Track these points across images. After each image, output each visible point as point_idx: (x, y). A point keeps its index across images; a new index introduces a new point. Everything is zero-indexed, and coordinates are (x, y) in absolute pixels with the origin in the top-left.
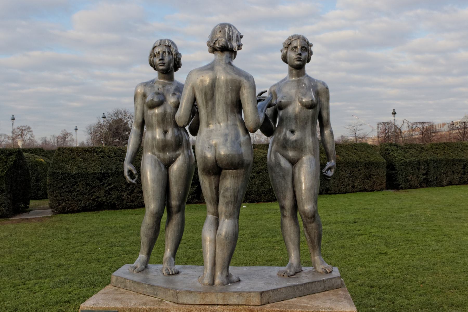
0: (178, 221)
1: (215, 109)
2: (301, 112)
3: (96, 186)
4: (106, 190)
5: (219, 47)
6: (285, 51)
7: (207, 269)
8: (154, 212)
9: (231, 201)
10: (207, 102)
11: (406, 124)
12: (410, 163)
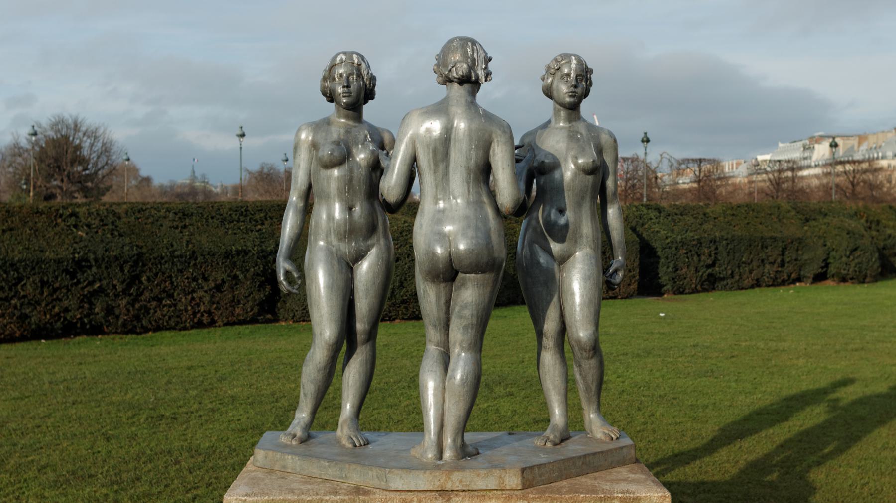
3: (63, 288)
4: (83, 295)
6: (549, 80)
7: (430, 434)
10: (436, 165)
12: (683, 243)
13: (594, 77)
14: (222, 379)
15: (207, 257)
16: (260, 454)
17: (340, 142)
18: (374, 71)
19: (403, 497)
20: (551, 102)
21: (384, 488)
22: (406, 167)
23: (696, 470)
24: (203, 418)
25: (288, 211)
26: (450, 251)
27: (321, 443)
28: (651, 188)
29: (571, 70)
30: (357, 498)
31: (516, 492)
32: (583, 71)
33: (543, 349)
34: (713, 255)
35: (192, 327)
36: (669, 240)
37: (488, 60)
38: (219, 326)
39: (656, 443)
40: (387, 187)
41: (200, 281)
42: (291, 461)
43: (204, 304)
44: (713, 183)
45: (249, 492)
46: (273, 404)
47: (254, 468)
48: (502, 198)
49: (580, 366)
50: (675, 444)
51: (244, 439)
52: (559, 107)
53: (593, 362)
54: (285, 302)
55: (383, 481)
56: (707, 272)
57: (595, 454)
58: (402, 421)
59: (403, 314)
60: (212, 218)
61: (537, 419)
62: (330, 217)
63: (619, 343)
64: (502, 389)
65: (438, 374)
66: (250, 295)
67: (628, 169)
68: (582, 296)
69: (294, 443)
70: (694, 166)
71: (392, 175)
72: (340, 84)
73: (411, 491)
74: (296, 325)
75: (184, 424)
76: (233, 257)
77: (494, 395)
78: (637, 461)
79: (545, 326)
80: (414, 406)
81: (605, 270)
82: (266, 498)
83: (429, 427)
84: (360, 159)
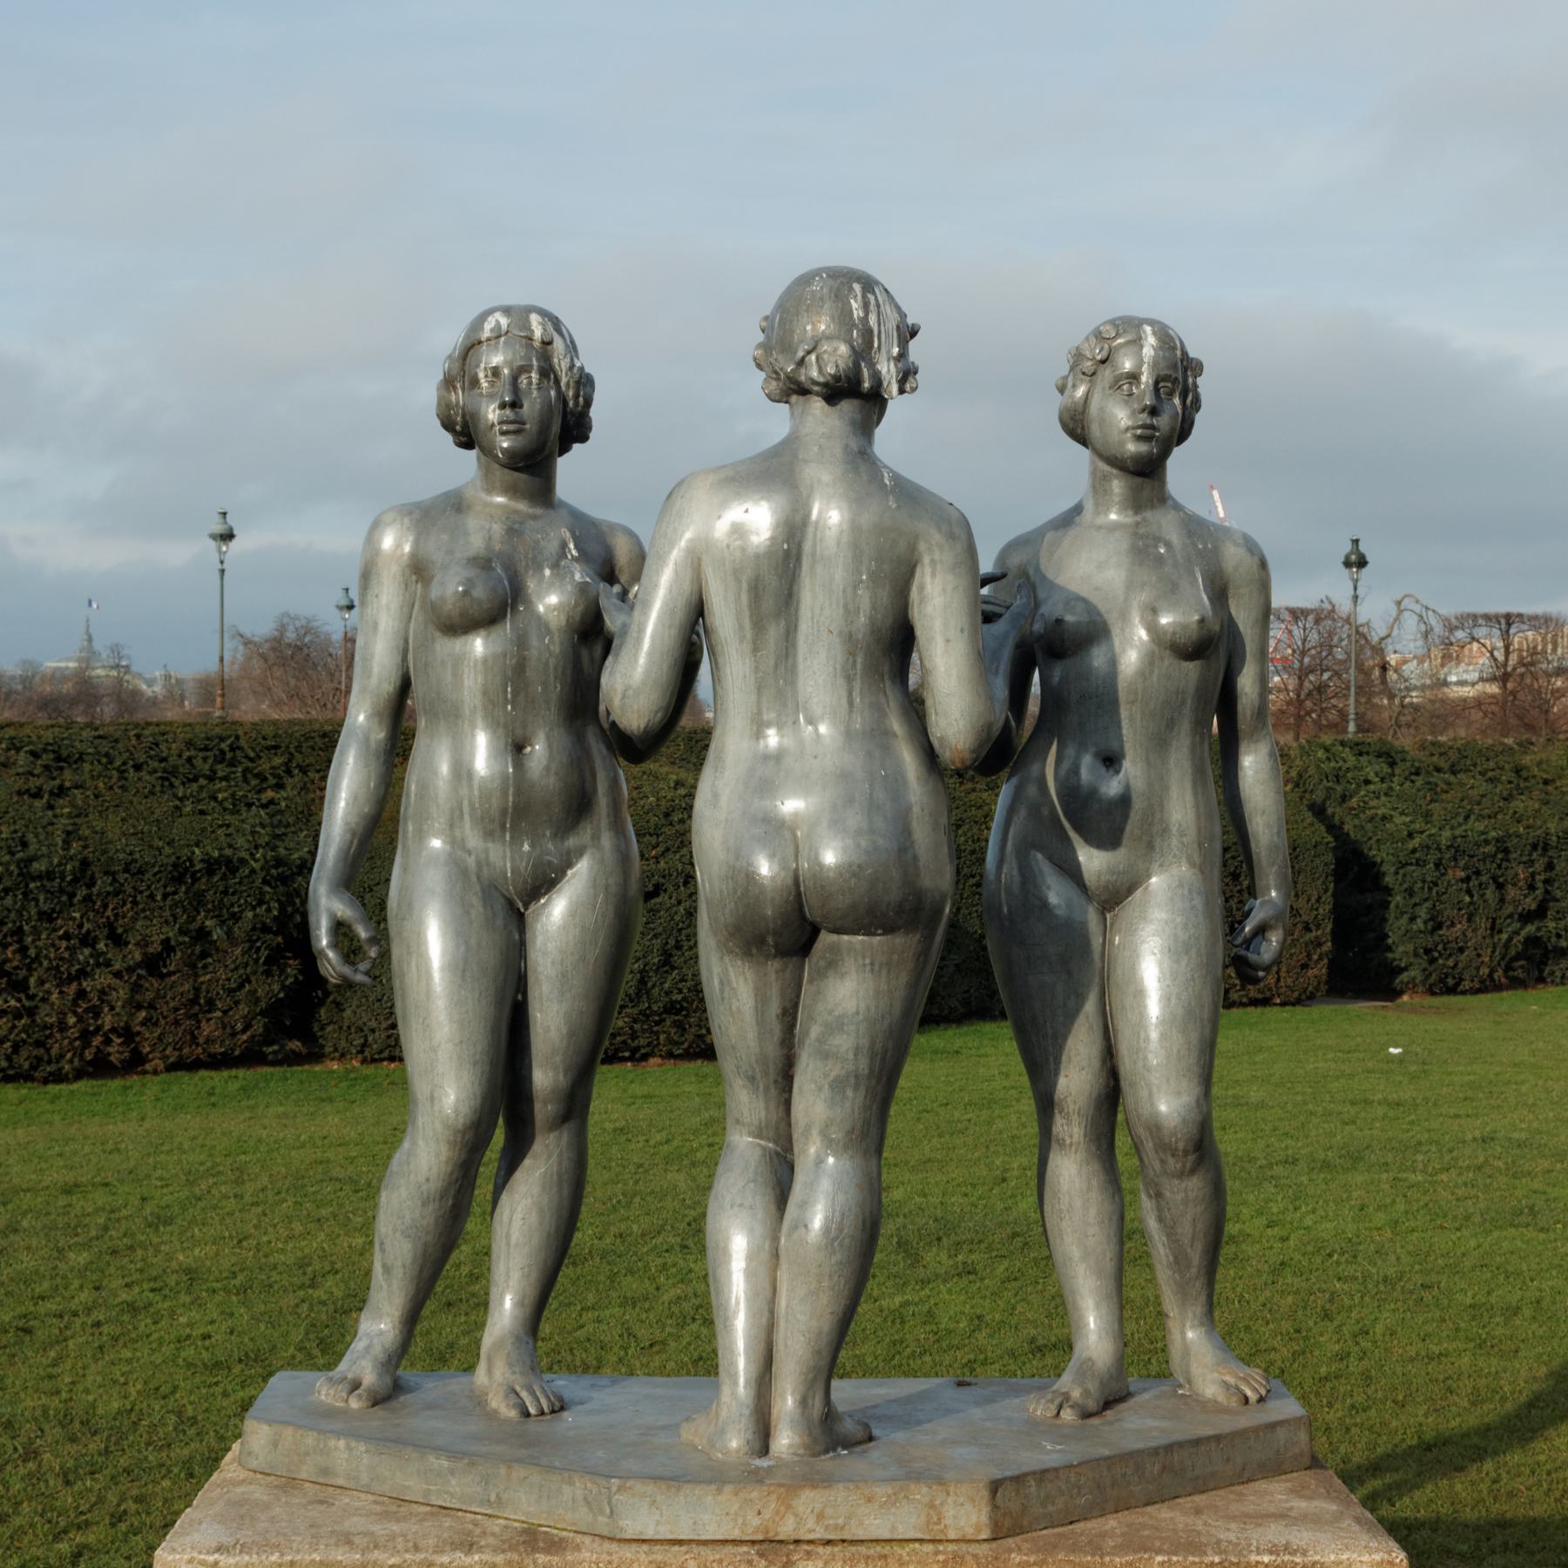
0: (560, 1164)
1: (795, 655)
2: (1152, 672)
5: (821, 380)
6: (1080, 392)
7: (736, 1383)
8: (461, 1121)
9: (856, 1077)
10: (759, 626)
11: (1416, 618)
12: (1457, 851)
13: (1204, 384)
14: (161, 1220)
15: (122, 877)
16: (258, 1436)
17: (489, 560)
18: (588, 361)
19: (659, 1558)
20: (1084, 454)
21: (605, 1533)
22: (674, 632)
23: (1484, 1487)
24: (105, 1329)
25: (342, 754)
26: (796, 870)
27: (430, 1406)
28: (1370, 695)
29: (1141, 363)
30: (528, 1561)
31: (974, 1548)
32: (1175, 367)
33: (1054, 1146)
34: (1540, 885)
35: (79, 1075)
36: (1415, 842)
37: (909, 333)
38: (155, 1072)
39: (1373, 1412)
40: (619, 688)
41: (101, 946)
42: (346, 1455)
43: (112, 1008)
44: (1543, 682)
45: (227, 1540)
46: (301, 1293)
47: (243, 1474)
48: (943, 723)
49: (1158, 1195)
50: (1426, 1415)
51: (218, 1390)
52: (1107, 468)
53: (1196, 1185)
54: (339, 1006)
55: (601, 1512)
56: (1523, 933)
57: (1197, 1442)
58: (664, 1343)
59: (670, 1041)
60: (138, 768)
61: (1041, 1342)
62: (462, 771)
63: (1275, 1129)
64: (943, 1256)
65: (760, 1214)
66: (241, 986)
67: (1304, 641)
68: (1166, 999)
69: (354, 1404)
70: (1489, 636)
71: (636, 656)
72: (491, 396)
73: (680, 1542)
74: (370, 1070)
75: (52, 1345)
76: (195, 880)
77: (921, 1273)
78: (1315, 1463)
79: (1062, 1082)
80: (697, 1302)
81: (1233, 923)
82: (274, 1558)
83: (734, 1364)
84: (548, 608)
